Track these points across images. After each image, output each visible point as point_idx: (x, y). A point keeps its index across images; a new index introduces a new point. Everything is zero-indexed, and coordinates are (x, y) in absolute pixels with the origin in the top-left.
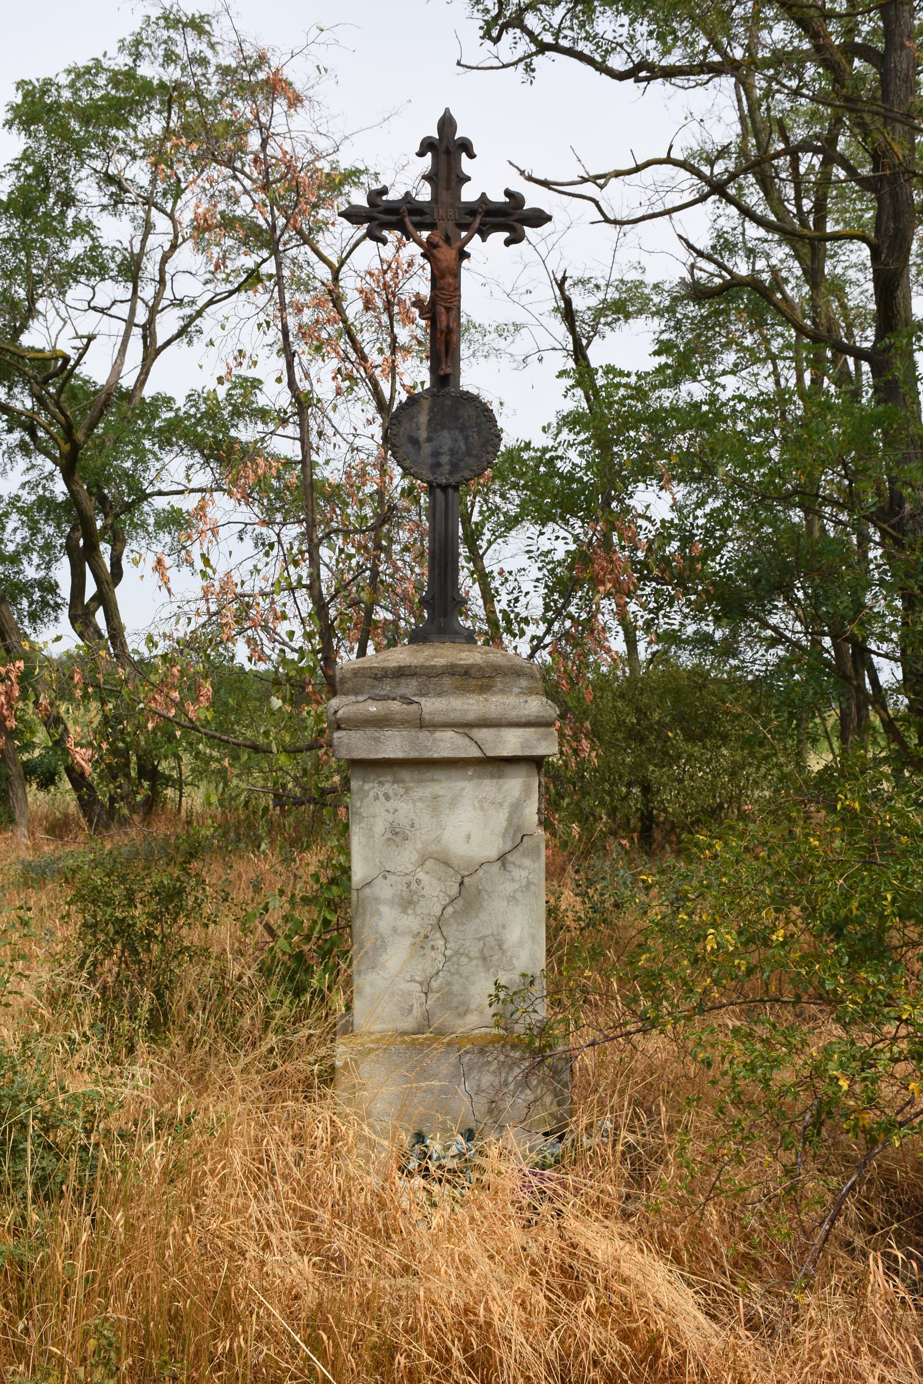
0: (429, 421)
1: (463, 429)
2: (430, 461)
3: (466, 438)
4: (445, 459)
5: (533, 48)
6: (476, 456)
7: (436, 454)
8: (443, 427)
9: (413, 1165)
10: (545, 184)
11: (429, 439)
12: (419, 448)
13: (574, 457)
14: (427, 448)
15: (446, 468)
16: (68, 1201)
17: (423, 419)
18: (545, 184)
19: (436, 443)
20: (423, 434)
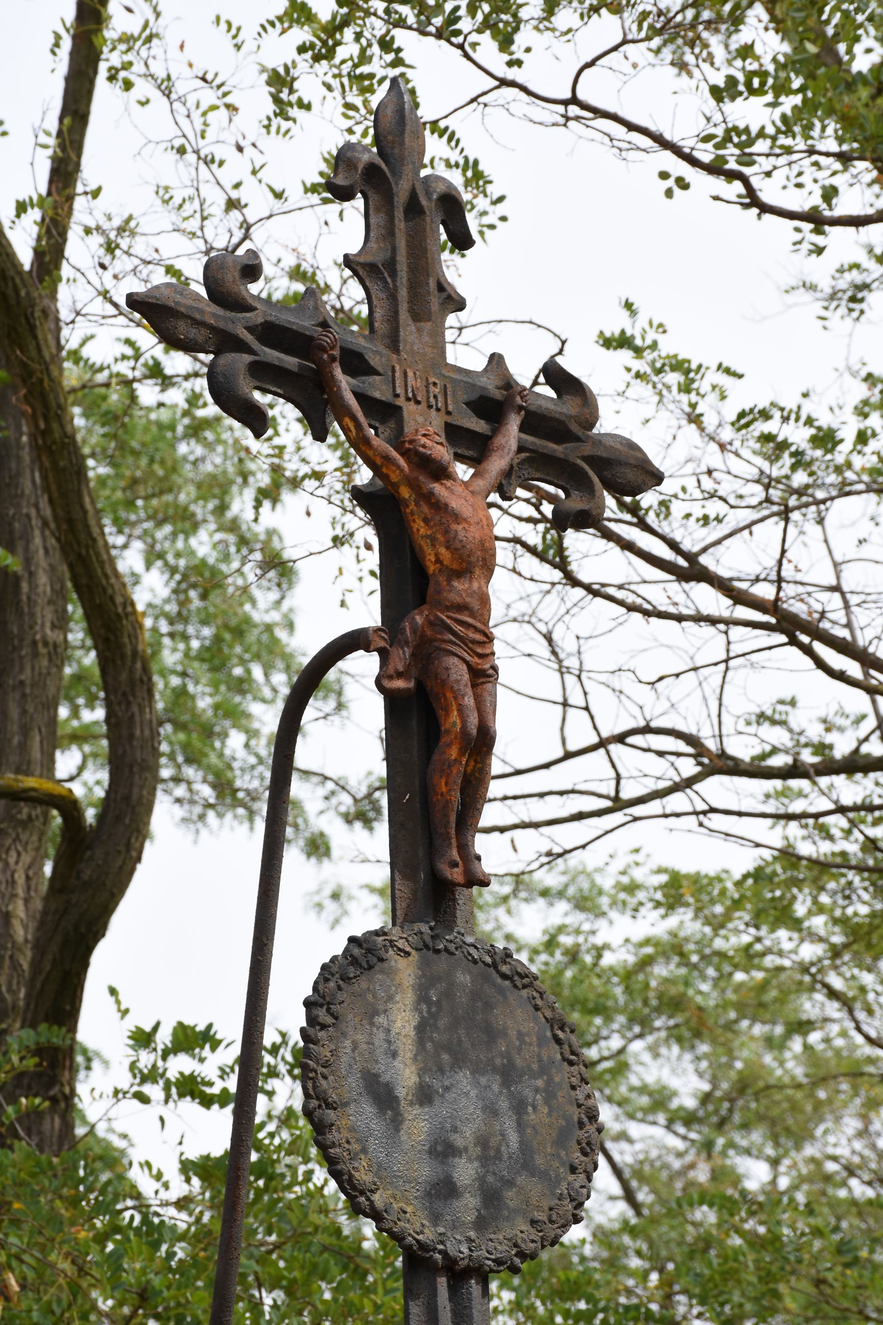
0: (421, 1029)
1: (508, 1074)
2: (425, 1171)
3: (519, 1107)
4: (465, 1172)
5: (136, 385)
6: (543, 1175)
7: (443, 1150)
8: (459, 1060)
9: (690, 34)
10: (645, 650)
11: (425, 1096)
12: (396, 1122)
13: (732, 1233)
14: (418, 1125)
15: (468, 1205)
16: (477, 572)
17: (403, 1020)
18: (645, 650)
19: (441, 1109)
20: (405, 1076)
